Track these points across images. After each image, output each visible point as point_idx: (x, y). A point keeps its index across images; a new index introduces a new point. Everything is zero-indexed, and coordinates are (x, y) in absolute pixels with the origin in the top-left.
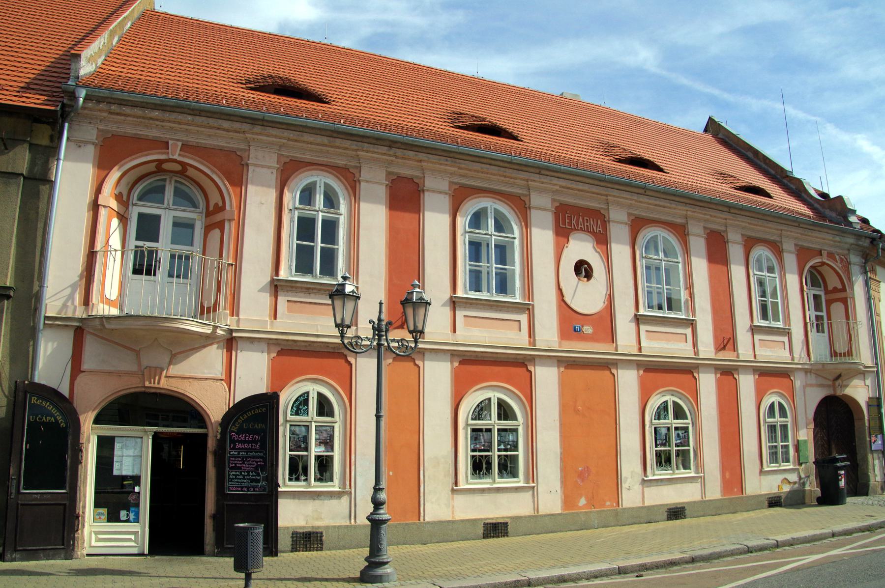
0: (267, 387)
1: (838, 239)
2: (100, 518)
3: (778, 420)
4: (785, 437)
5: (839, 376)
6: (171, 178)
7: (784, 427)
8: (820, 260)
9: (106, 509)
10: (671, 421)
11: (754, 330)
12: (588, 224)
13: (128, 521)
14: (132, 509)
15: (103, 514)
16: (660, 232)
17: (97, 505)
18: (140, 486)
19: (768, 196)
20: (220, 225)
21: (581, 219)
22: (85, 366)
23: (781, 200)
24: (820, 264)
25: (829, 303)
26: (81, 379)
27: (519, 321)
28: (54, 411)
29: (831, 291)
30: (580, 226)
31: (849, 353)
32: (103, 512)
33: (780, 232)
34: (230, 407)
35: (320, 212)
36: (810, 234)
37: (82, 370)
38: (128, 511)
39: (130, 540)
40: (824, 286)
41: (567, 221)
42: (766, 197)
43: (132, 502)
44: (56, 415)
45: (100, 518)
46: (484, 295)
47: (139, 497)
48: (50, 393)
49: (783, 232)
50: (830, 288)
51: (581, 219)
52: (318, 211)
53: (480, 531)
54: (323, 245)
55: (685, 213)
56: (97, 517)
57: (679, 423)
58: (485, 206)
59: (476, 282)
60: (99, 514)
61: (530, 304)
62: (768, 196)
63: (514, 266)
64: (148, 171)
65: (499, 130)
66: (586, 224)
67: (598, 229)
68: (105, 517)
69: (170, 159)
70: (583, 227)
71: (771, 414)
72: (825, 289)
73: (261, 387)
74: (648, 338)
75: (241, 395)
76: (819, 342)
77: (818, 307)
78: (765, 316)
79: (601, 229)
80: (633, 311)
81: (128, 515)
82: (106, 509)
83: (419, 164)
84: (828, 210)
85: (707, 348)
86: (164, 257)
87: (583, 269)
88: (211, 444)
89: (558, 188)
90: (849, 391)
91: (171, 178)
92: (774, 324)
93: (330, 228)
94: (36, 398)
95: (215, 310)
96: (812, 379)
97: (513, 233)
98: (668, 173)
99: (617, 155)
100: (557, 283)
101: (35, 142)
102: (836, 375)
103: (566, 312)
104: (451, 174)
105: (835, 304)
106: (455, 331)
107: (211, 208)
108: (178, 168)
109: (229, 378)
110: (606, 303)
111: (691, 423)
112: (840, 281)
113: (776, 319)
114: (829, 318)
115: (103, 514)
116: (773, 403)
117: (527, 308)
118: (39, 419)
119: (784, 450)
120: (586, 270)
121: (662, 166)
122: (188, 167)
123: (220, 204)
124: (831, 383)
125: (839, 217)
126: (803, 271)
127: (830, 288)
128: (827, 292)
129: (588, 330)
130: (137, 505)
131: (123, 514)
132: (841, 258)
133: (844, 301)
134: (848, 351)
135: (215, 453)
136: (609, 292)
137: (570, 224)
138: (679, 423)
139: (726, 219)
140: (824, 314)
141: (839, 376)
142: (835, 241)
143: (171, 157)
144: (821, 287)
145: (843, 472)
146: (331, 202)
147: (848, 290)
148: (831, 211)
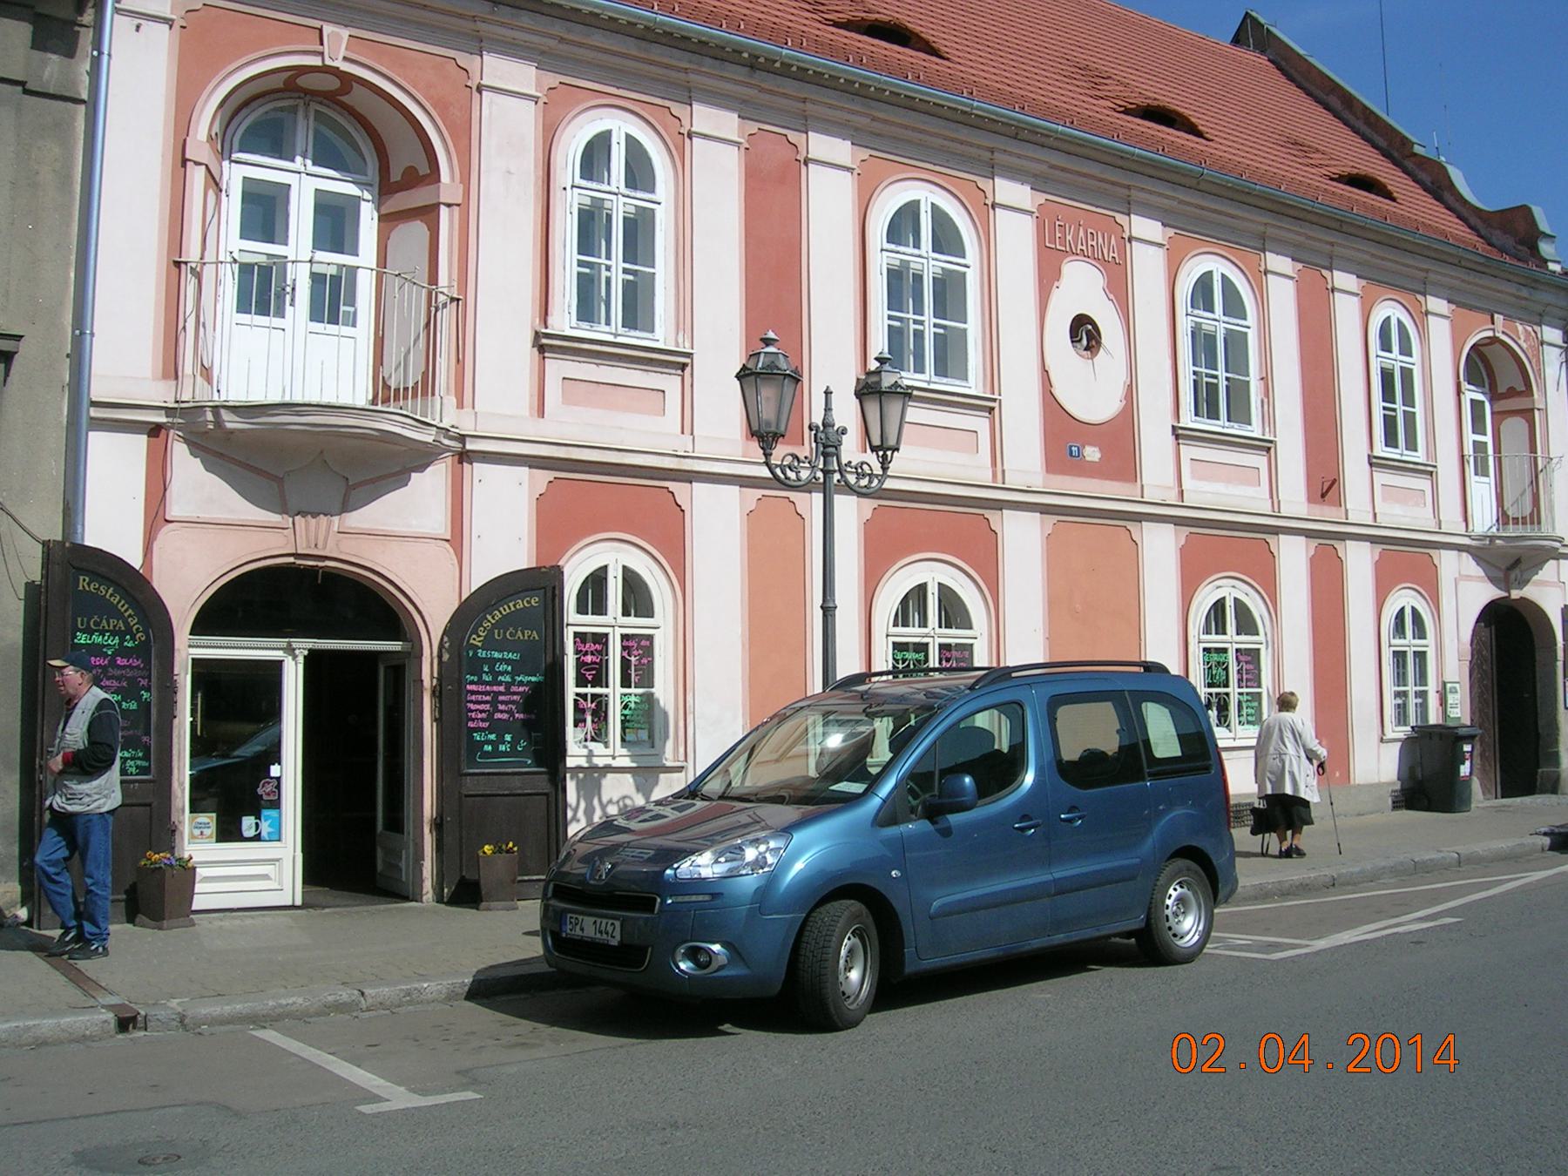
0: (529, 558)
1: (1524, 292)
2: (202, 833)
3: (1409, 643)
4: (1422, 678)
5: (1518, 562)
6: (307, 105)
7: (1421, 656)
8: (1490, 334)
9: (214, 815)
10: (1232, 639)
11: (1374, 462)
12: (1094, 243)
13: (257, 838)
14: (265, 813)
15: (207, 825)
16: (928, 194)
17: (194, 809)
18: (279, 764)
19: (1389, 196)
20: (429, 213)
21: (1081, 234)
22: (175, 510)
23: (1413, 203)
24: (1488, 341)
25: (1498, 416)
26: (165, 535)
27: (663, 392)
28: (123, 607)
29: (1502, 394)
30: (1080, 247)
31: (1535, 518)
32: (206, 820)
33: (988, 155)
34: (464, 598)
35: (620, 196)
36: (1477, 280)
37: (168, 518)
38: (258, 817)
39: (266, 877)
40: (1490, 384)
41: (1058, 235)
42: (1386, 198)
43: (265, 797)
44: (126, 614)
45: (202, 833)
46: (600, 332)
47: (278, 787)
48: (107, 566)
49: (996, 154)
50: (1502, 389)
51: (1081, 234)
52: (616, 194)
53: (469, 875)
54: (1247, 379)
55: (1262, 228)
56: (197, 832)
57: (1246, 641)
58: (916, 198)
59: (588, 304)
60: (199, 826)
61: (995, 400)
62: (1389, 196)
63: (1414, 407)
64: (269, 88)
65: (908, 34)
66: (1090, 243)
67: (1111, 254)
68: (211, 831)
69: (325, 66)
70: (1084, 248)
71: (1397, 631)
72: (1490, 390)
73: (519, 556)
74: (1195, 476)
75: (479, 577)
76: (1482, 491)
77: (1478, 427)
78: (1391, 440)
79: (1115, 255)
80: (1169, 421)
81: (257, 824)
82: (214, 815)
83: (801, 105)
84: (1498, 232)
85: (1295, 500)
86: (300, 277)
87: (1084, 332)
88: (428, 672)
89: (1044, 168)
90: (1529, 592)
91: (307, 105)
92: (1410, 456)
93: (639, 231)
94: (87, 579)
95: (425, 393)
96: (1469, 565)
97: (1245, 318)
98: (948, 59)
99: (1117, 97)
100: (1040, 361)
101: (39, 10)
102: (1512, 561)
103: (1055, 414)
104: (856, 129)
105: (1527, 425)
106: (541, 412)
107: (396, 176)
108: (333, 84)
109: (457, 539)
110: (1124, 402)
111: (1264, 641)
112: (1522, 373)
113: (1412, 445)
114: (1497, 449)
115: (207, 825)
116: (1402, 610)
117: (987, 407)
118: (511, 634)
119: (1419, 701)
120: (1088, 333)
121: (940, 44)
122: (354, 84)
123: (424, 169)
124: (1501, 575)
125: (1520, 247)
126: (1461, 353)
127: (1502, 389)
128: (1494, 397)
129: (1092, 454)
130: (276, 804)
131: (248, 823)
132: (1526, 331)
133: (1527, 414)
134: (1532, 514)
135: (437, 693)
136: (1129, 383)
137: (1063, 239)
138: (1246, 641)
139: (1332, 244)
140: (1488, 439)
141: (1518, 562)
142: (1518, 297)
143: (328, 62)
144: (1484, 387)
145: (1467, 748)
146: (639, 173)
147: (1536, 396)
148: (1505, 233)
